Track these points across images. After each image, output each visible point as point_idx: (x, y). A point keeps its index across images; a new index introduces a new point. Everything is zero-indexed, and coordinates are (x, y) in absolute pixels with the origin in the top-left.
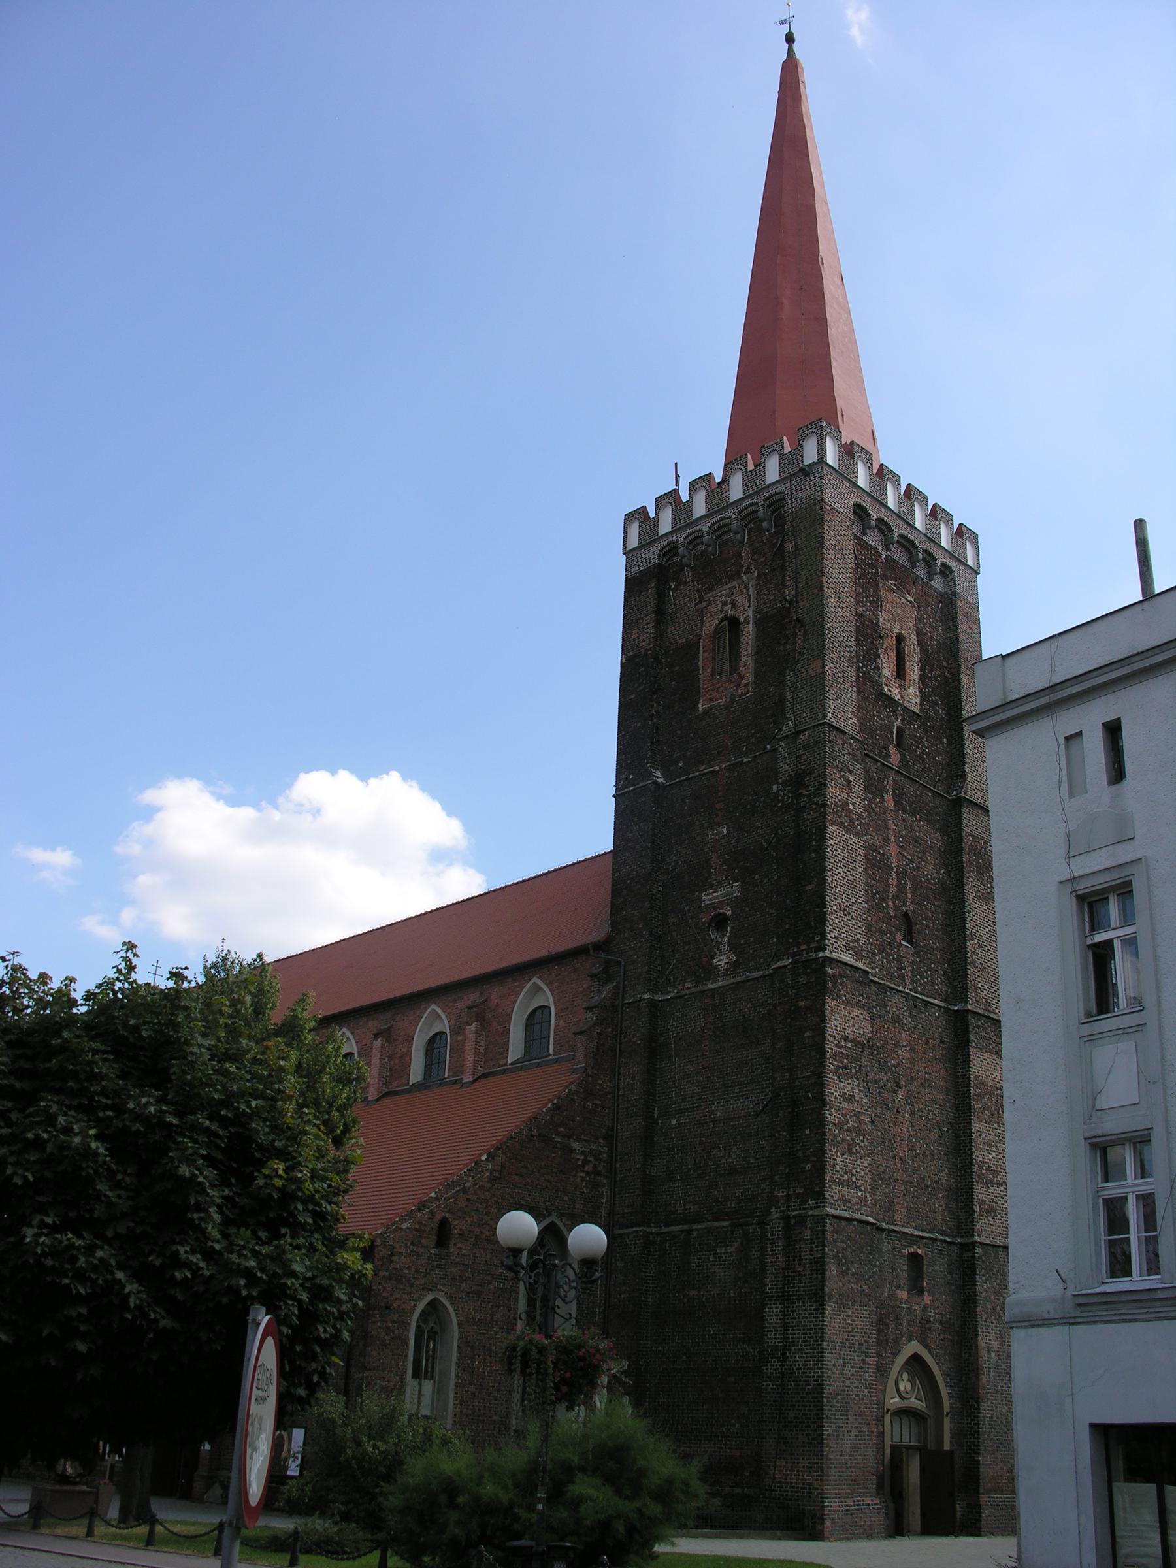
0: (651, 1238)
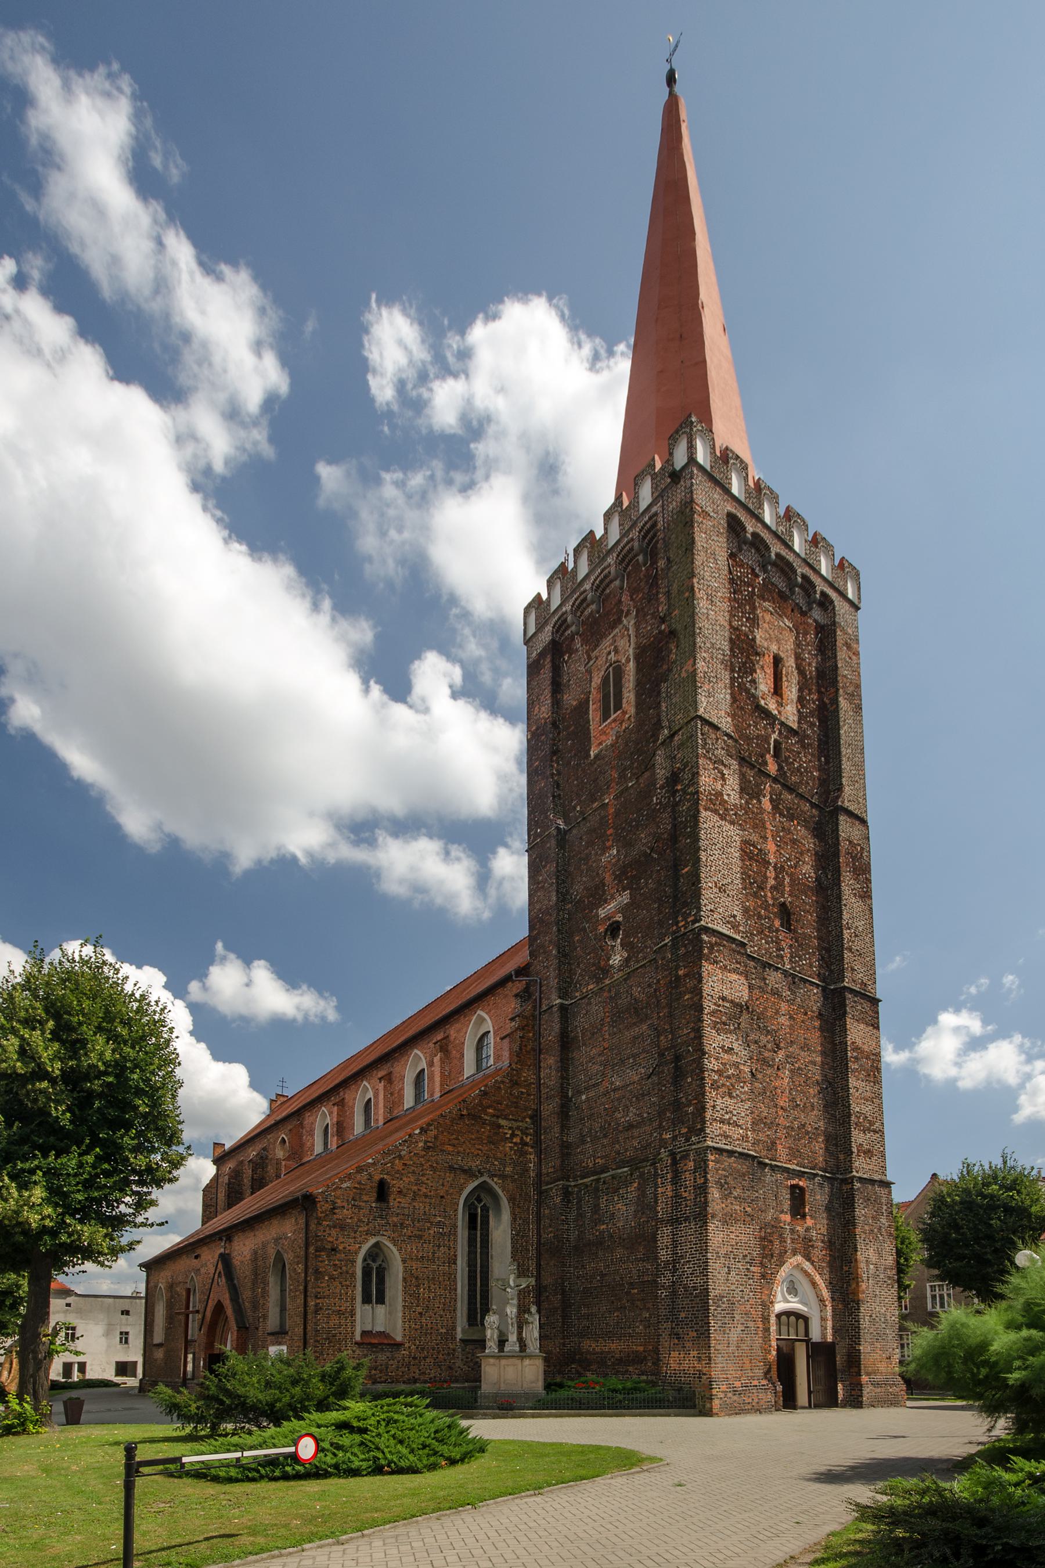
0: (570, 1189)
